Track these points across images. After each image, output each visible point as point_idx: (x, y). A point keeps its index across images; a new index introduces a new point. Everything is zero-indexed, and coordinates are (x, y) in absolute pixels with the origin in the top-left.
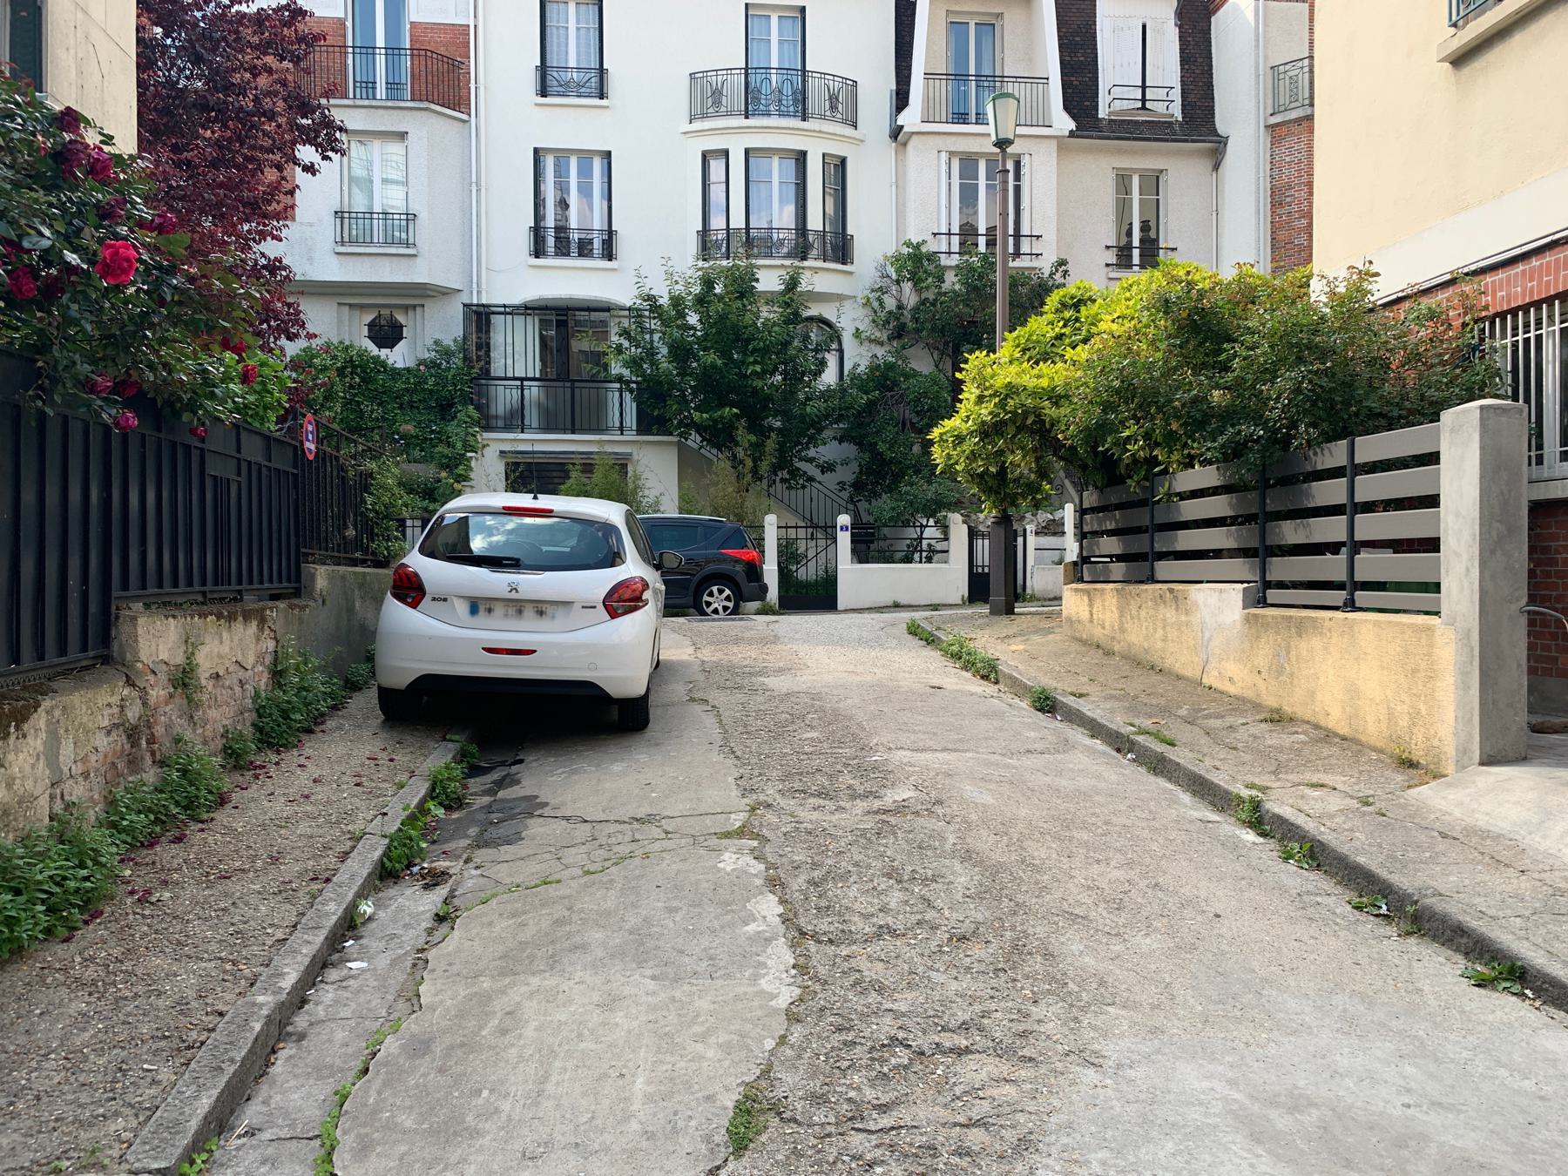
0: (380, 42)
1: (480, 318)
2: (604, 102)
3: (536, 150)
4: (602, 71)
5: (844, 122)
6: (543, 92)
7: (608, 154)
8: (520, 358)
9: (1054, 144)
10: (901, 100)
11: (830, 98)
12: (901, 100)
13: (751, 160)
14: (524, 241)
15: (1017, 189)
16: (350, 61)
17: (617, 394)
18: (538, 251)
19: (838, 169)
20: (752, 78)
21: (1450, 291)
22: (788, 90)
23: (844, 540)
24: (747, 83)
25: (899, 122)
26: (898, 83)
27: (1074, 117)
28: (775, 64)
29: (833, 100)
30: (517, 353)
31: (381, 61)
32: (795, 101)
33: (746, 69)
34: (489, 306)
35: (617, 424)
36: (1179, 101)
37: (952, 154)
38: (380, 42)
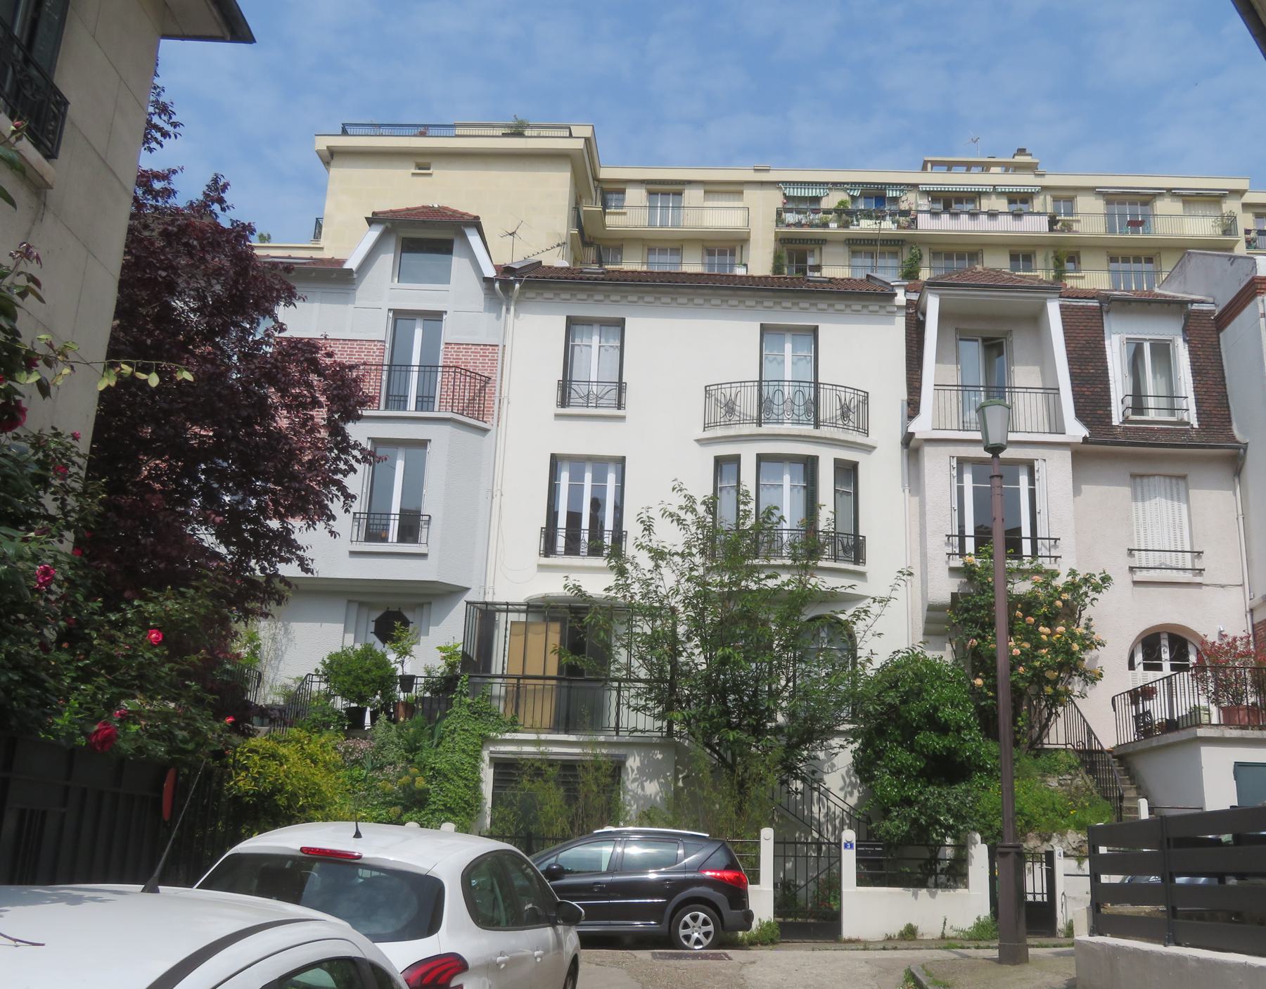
0: (416, 360)
1: (485, 615)
2: (620, 413)
3: (553, 457)
4: (621, 387)
5: (857, 429)
6: (564, 401)
7: (621, 462)
8: (1027, 402)
9: (1067, 455)
10: (913, 407)
11: (842, 407)
12: (913, 407)
13: (530, 636)
14: (535, 541)
15: (1032, 493)
16: (384, 377)
17: (614, 693)
18: (549, 548)
19: (847, 472)
20: (765, 389)
21: (541, 682)
22: (800, 400)
23: (849, 859)
24: (760, 395)
25: (910, 430)
26: (909, 393)
27: (1087, 424)
28: (788, 376)
29: (845, 412)
30: (521, 654)
31: (414, 377)
32: (807, 411)
33: (761, 381)
34: (494, 604)
35: (613, 724)
36: (1193, 409)
37: (962, 462)
38: (416, 360)
